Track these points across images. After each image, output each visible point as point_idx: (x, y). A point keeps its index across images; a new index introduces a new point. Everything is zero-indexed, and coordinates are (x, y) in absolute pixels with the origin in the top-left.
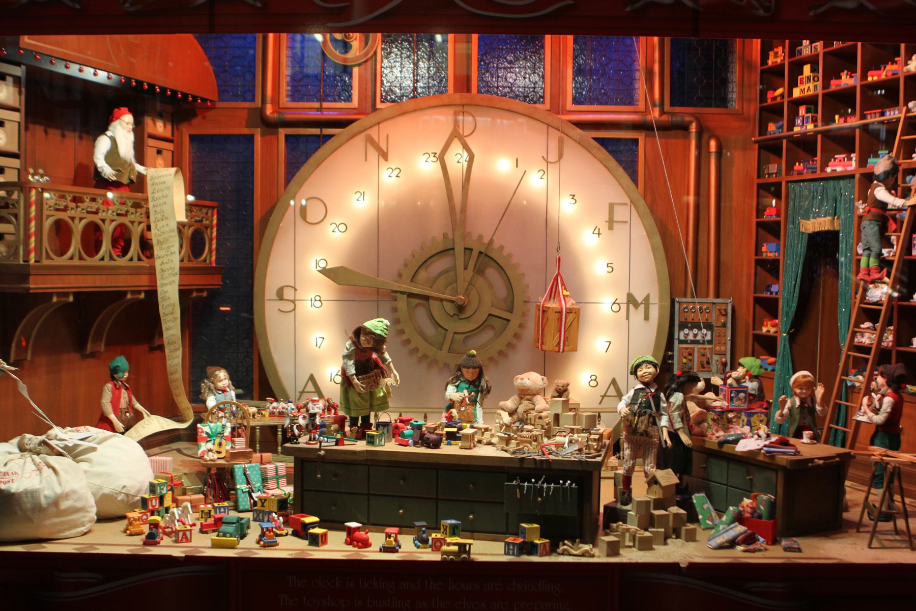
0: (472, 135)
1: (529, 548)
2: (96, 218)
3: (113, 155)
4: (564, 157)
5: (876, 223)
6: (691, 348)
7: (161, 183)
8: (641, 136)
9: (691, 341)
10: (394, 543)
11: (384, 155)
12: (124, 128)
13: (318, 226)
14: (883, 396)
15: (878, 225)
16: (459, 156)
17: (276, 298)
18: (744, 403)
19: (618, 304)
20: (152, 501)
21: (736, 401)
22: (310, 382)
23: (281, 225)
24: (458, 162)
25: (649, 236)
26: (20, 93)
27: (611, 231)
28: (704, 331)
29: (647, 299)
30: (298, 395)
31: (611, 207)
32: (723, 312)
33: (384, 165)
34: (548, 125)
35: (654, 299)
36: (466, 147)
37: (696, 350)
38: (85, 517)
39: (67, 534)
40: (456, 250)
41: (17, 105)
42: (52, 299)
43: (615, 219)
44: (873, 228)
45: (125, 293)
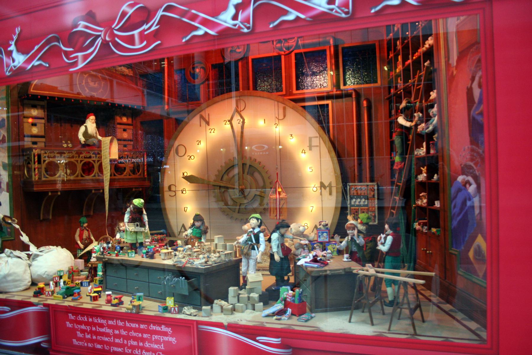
0: (245, 110)
1: (166, 309)
2: (90, 160)
3: (86, 134)
4: (286, 116)
5: (399, 137)
6: (357, 209)
7: (106, 143)
8: (329, 102)
9: (357, 205)
10: (304, 294)
11: (208, 123)
12: (90, 122)
13: (182, 157)
14: (388, 235)
15: (401, 138)
16: (239, 120)
17: (168, 190)
18: (326, 238)
19: (316, 187)
20: (55, 278)
21: (322, 237)
22: (183, 228)
23: (169, 158)
24: (239, 123)
25: (329, 152)
26: (44, 112)
27: (310, 151)
28: (363, 200)
29: (330, 185)
30: (178, 233)
31: (310, 139)
32: (373, 190)
33: (208, 127)
34: (278, 102)
35: (334, 184)
36: (242, 117)
37: (360, 210)
38: (21, 283)
39: (13, 290)
40: (42, 168)
41: (43, 116)
42: (48, 194)
43: (313, 145)
44: (398, 140)
45: (132, 189)
